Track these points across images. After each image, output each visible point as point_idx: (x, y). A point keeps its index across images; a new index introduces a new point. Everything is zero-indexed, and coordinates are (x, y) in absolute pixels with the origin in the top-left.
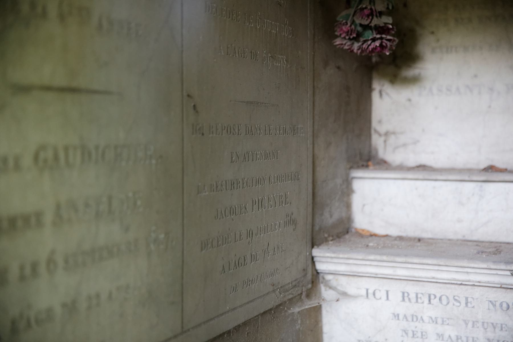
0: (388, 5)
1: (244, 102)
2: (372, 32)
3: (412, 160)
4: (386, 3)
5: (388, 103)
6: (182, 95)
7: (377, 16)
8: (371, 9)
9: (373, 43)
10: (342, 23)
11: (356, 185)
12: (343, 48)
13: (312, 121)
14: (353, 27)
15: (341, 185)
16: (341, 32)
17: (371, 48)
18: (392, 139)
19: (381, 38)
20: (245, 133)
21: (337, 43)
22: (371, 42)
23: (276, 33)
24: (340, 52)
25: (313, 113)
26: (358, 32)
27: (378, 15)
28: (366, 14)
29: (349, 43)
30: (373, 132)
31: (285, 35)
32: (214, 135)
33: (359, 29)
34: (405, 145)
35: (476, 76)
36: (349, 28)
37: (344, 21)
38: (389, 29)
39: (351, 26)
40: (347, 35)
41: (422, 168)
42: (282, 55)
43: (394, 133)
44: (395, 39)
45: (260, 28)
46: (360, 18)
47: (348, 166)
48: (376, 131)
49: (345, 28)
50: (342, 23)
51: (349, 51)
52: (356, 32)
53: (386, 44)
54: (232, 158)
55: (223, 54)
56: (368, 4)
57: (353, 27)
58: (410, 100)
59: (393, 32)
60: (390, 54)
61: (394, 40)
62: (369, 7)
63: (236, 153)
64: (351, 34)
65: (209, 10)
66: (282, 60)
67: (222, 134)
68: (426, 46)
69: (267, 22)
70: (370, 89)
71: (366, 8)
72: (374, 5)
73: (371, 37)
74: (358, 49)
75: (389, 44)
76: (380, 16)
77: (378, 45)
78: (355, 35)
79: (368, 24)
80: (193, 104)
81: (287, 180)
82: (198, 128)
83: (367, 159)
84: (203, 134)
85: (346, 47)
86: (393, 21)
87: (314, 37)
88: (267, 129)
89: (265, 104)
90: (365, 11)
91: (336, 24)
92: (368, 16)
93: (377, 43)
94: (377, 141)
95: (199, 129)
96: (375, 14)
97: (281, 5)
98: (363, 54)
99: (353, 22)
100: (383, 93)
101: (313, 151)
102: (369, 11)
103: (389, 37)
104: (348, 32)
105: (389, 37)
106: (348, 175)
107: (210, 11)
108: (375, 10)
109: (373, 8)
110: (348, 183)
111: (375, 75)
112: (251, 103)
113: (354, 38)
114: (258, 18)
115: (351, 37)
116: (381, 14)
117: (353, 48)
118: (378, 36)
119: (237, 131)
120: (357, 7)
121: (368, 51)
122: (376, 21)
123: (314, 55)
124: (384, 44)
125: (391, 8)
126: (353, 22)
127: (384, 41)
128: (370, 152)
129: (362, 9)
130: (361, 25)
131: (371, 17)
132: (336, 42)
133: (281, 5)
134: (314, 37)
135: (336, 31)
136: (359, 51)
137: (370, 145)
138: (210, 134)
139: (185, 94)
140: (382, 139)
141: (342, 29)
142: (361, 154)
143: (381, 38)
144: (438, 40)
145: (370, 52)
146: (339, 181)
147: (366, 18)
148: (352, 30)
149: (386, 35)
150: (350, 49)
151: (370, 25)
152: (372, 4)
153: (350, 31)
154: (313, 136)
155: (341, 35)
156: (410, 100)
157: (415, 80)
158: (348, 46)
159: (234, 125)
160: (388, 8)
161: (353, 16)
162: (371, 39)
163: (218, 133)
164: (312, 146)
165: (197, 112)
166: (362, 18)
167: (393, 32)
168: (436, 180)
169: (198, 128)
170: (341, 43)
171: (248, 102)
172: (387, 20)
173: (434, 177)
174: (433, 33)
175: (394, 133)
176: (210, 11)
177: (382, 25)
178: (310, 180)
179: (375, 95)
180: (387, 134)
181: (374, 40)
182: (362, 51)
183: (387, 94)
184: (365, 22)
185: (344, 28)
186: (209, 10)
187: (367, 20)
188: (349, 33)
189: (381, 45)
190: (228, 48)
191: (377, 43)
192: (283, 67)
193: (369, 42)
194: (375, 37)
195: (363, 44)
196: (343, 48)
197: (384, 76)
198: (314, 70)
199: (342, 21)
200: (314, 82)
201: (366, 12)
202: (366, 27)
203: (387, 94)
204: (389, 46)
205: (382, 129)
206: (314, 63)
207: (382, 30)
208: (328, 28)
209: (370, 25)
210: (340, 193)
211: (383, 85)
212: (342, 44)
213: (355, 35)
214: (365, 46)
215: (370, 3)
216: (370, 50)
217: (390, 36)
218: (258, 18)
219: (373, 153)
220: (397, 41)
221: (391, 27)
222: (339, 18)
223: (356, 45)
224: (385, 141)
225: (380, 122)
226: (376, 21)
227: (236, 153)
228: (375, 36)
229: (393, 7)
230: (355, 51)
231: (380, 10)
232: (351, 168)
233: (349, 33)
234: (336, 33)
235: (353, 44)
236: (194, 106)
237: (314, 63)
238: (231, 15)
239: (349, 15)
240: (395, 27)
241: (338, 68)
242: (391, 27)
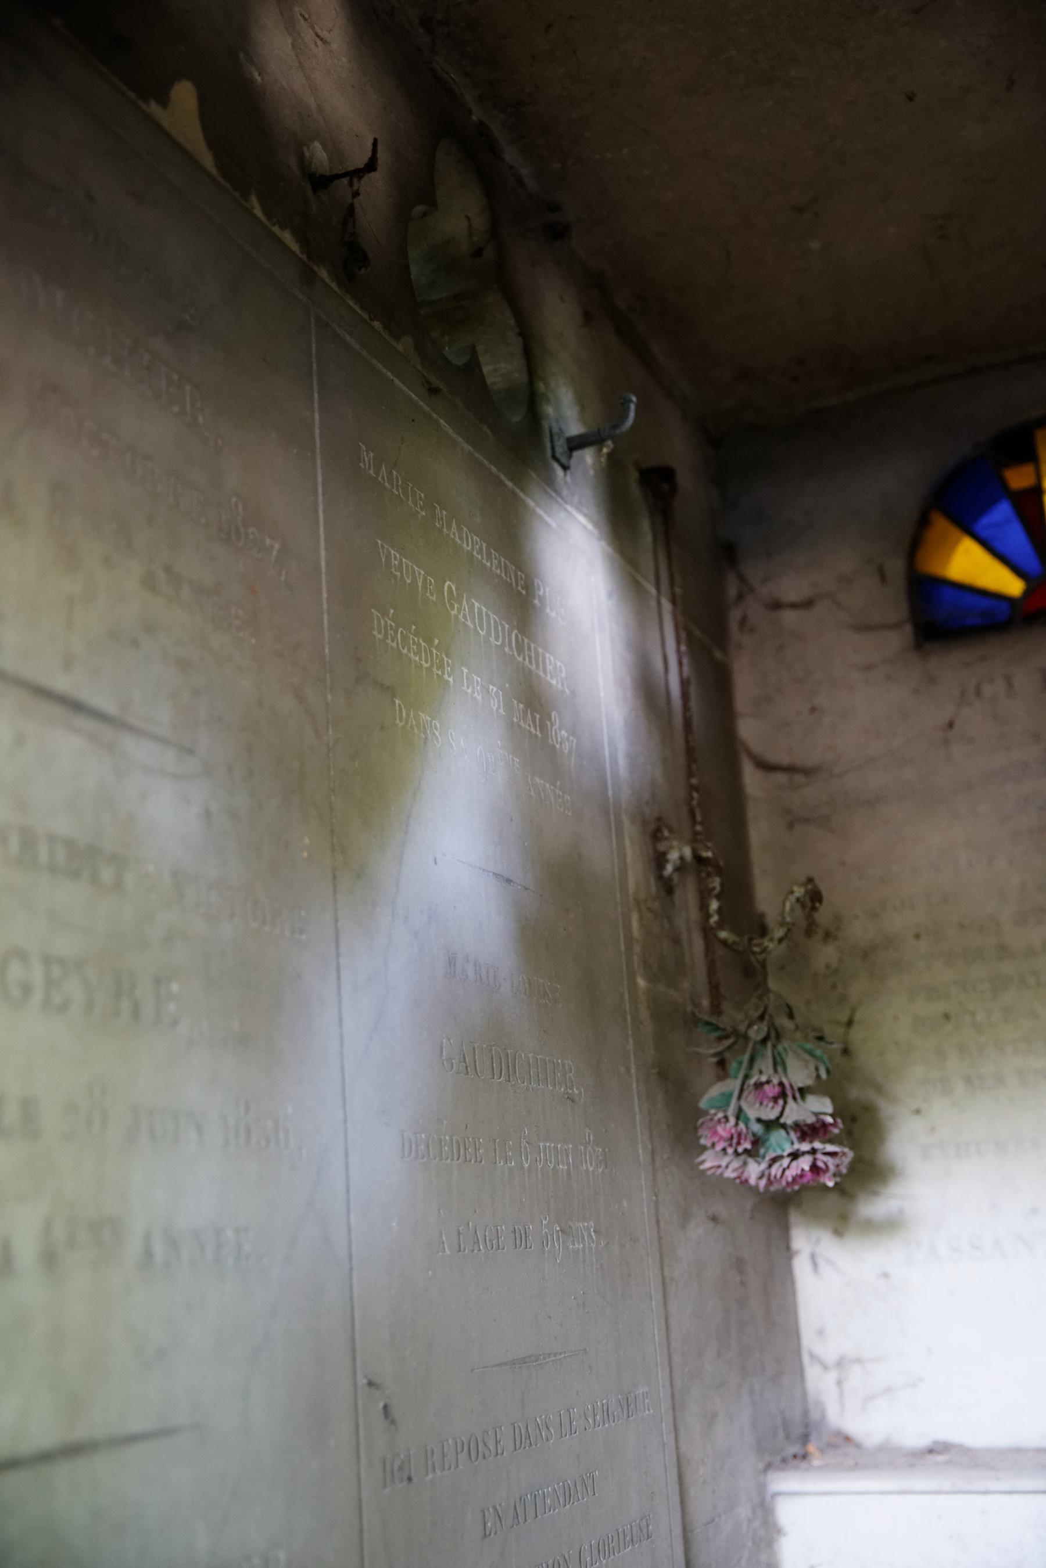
0: (817, 1069)
1: (506, 1364)
2: (788, 1133)
3: (914, 1435)
4: (812, 1068)
5: (831, 1279)
6: (355, 1386)
7: (794, 1098)
8: (781, 1084)
9: (794, 1163)
10: (716, 1118)
11: (787, 1512)
12: (721, 1174)
13: (668, 1370)
14: (742, 1126)
15: (750, 1521)
16: (716, 1139)
17: (790, 1174)
18: (855, 1376)
19: (813, 1151)
20: (512, 1446)
21: (707, 1165)
22: (787, 1161)
23: (569, 1169)
24: (714, 1184)
25: (669, 1348)
26: (754, 1135)
27: (798, 1095)
28: (771, 1095)
29: (736, 1164)
30: (806, 1359)
31: (587, 1170)
32: (438, 1473)
33: (757, 1128)
34: (888, 1390)
35: (1034, 1211)
36: (733, 1131)
37: (720, 1115)
38: (825, 1125)
39: (737, 1124)
40: (731, 1145)
41: (938, 1453)
42: (584, 1220)
43: (858, 1361)
44: (846, 1150)
45: (530, 1167)
46: (757, 1105)
47: (761, 1466)
48: (812, 1355)
49: (724, 1129)
50: (716, 1118)
51: (738, 1181)
52: (750, 1137)
53: (825, 1164)
54: (485, 1524)
55: (448, 1252)
56: (771, 1071)
57: (742, 1126)
58: (886, 1275)
59: (836, 1131)
60: (836, 1184)
61: (844, 1154)
62: (775, 1081)
63: (494, 1507)
64: (739, 1143)
65: (410, 1154)
66: (586, 1234)
67: (457, 1466)
68: (905, 1138)
69: (545, 1147)
70: (788, 1253)
71: (768, 1082)
72: (785, 1070)
73: (788, 1150)
74: (761, 1177)
75: (829, 1160)
76: (803, 1097)
77: (807, 1168)
78: (748, 1145)
79: (778, 1118)
80: (381, 1405)
81: (622, 1544)
82: (396, 1467)
83: (799, 1439)
84: (410, 1479)
85: (730, 1174)
86: (835, 1110)
87: (653, 1159)
88: (565, 1420)
89: (555, 1355)
90: (766, 1087)
91: (700, 1121)
92: (775, 1099)
93: (805, 1163)
94: (819, 1383)
95: (401, 1468)
96: (789, 1092)
97: (573, 1101)
98: (772, 1189)
99: (739, 1114)
100: (821, 1262)
101: (677, 1448)
102: (777, 1089)
103: (830, 1148)
104: (732, 1138)
105: (830, 1148)
106: (762, 1488)
107: (413, 1153)
108: (791, 1086)
109: (785, 1081)
110: (764, 1508)
111: (794, 1216)
112: (523, 1361)
113: (746, 1151)
114: (524, 1143)
115: (740, 1150)
116: (803, 1092)
117: (745, 1175)
118: (805, 1147)
119: (492, 1447)
120: (747, 1077)
121: (784, 1183)
122: (795, 1112)
123: (657, 1202)
124: (820, 1164)
125: (824, 1075)
126: (739, 1114)
127: (819, 1156)
128: (806, 1413)
129: (759, 1086)
130: (759, 1120)
131: (781, 1102)
132: (703, 1162)
133: (573, 1101)
134: (653, 1159)
135: (700, 1137)
136: (763, 1183)
137: (804, 1393)
138: (427, 1474)
139: (362, 1381)
140: (832, 1376)
141: (715, 1133)
142: (786, 1425)
143: (813, 1151)
144: (933, 1129)
145: (788, 1184)
146: (743, 1511)
147: (771, 1104)
148: (739, 1135)
149: (824, 1142)
150: (739, 1177)
151: (782, 1121)
152: (780, 1069)
153: (735, 1136)
154: (674, 1409)
155: (713, 1145)
156: (886, 1275)
157: (889, 1227)
158: (735, 1170)
159: (486, 1432)
160: (818, 1077)
161: (740, 1097)
162: (789, 1155)
163: (447, 1466)
164: (673, 1435)
165: (393, 1422)
166: (761, 1103)
167: (836, 1131)
168: (986, 1493)
169: (396, 1467)
170: (716, 1163)
171: (513, 1363)
172: (820, 1106)
173: (981, 1485)
174: (918, 1112)
175: (858, 1361)
176: (413, 1153)
177: (811, 1120)
178: (677, 1531)
179: (801, 1266)
180: (841, 1363)
181: (795, 1156)
182: (770, 1182)
183: (830, 1262)
184: (771, 1114)
185: (720, 1129)
186: (410, 1154)
187: (773, 1108)
188: (735, 1141)
189: (815, 1168)
190: (459, 1233)
191: (805, 1163)
192: (591, 1249)
193: (786, 1162)
194: (798, 1150)
195: (770, 1166)
196: (721, 1174)
197: (817, 1218)
198: (660, 1239)
199: (715, 1114)
200: (662, 1270)
201: (771, 1090)
202: (770, 1125)
203: (830, 1262)
204: (832, 1168)
205: (829, 1351)
206: (658, 1222)
207: (809, 1131)
208: (682, 1127)
209: (782, 1121)
210: (750, 1544)
211: (818, 1242)
212: (719, 1167)
213: (748, 1145)
214: (775, 1170)
215: (776, 1070)
216: (790, 1179)
217: (831, 1141)
218: (524, 1143)
219: (815, 1415)
220: (851, 1154)
221: (830, 1120)
222: (703, 1104)
223: (754, 1170)
224: (839, 1383)
225: (821, 1333)
226: (795, 1112)
227: (494, 1507)
228: (797, 1146)
229: (828, 1072)
230: (752, 1181)
231: (800, 1085)
232: (768, 1467)
233: (735, 1141)
234: (702, 1141)
235: (745, 1164)
236: (385, 1407)
237: (658, 1222)
238: (462, 1152)
239: (731, 1095)
240: (839, 1121)
241: (714, 1219)
242: (830, 1120)
